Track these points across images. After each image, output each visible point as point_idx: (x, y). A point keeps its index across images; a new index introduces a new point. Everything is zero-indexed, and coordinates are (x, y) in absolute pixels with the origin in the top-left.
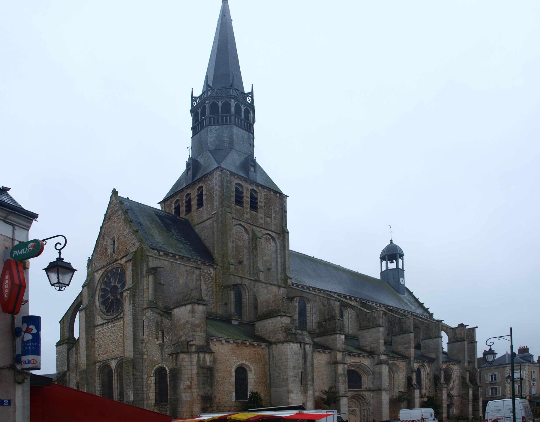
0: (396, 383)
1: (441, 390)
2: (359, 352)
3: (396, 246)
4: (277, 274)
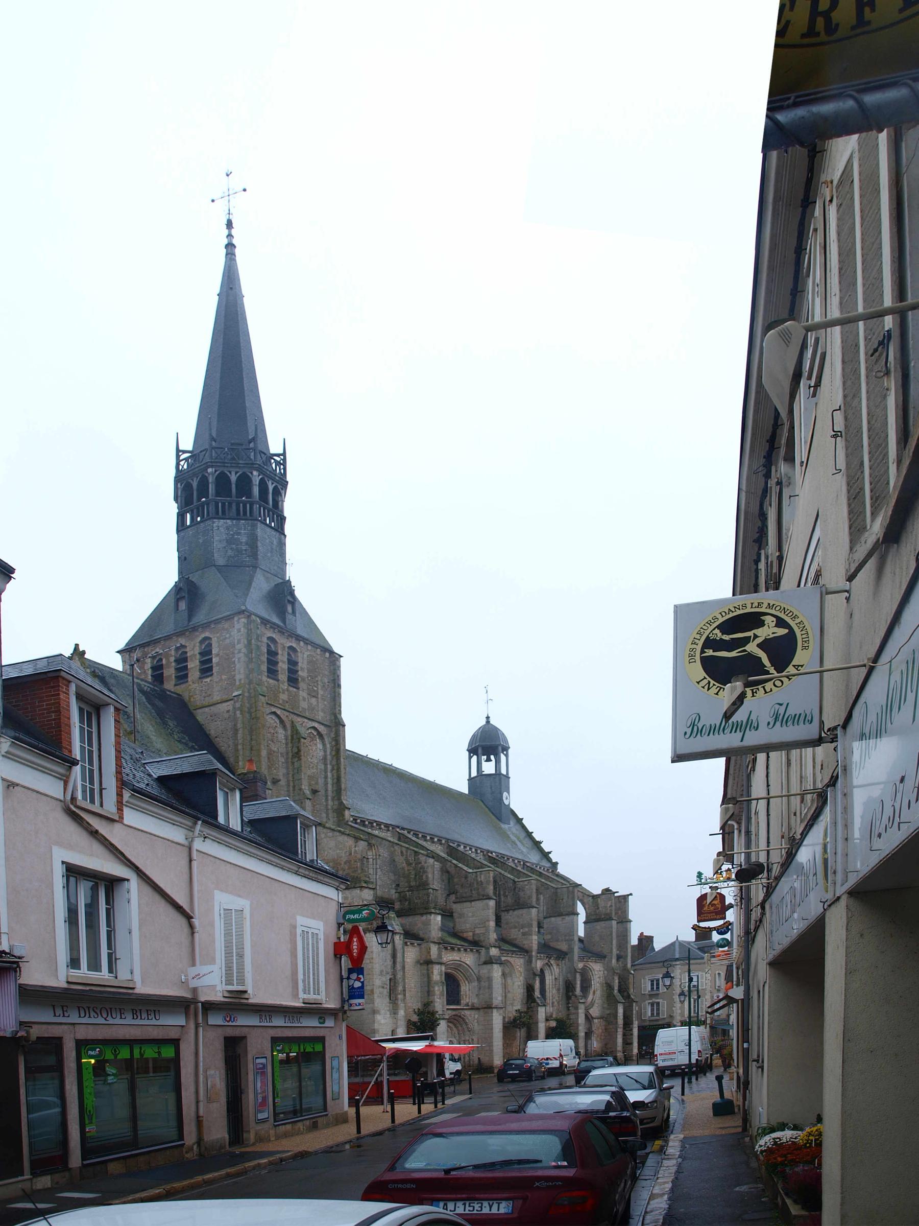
0: (509, 995)
1: (577, 1008)
2: (458, 942)
3: (496, 730)
4: (327, 800)
